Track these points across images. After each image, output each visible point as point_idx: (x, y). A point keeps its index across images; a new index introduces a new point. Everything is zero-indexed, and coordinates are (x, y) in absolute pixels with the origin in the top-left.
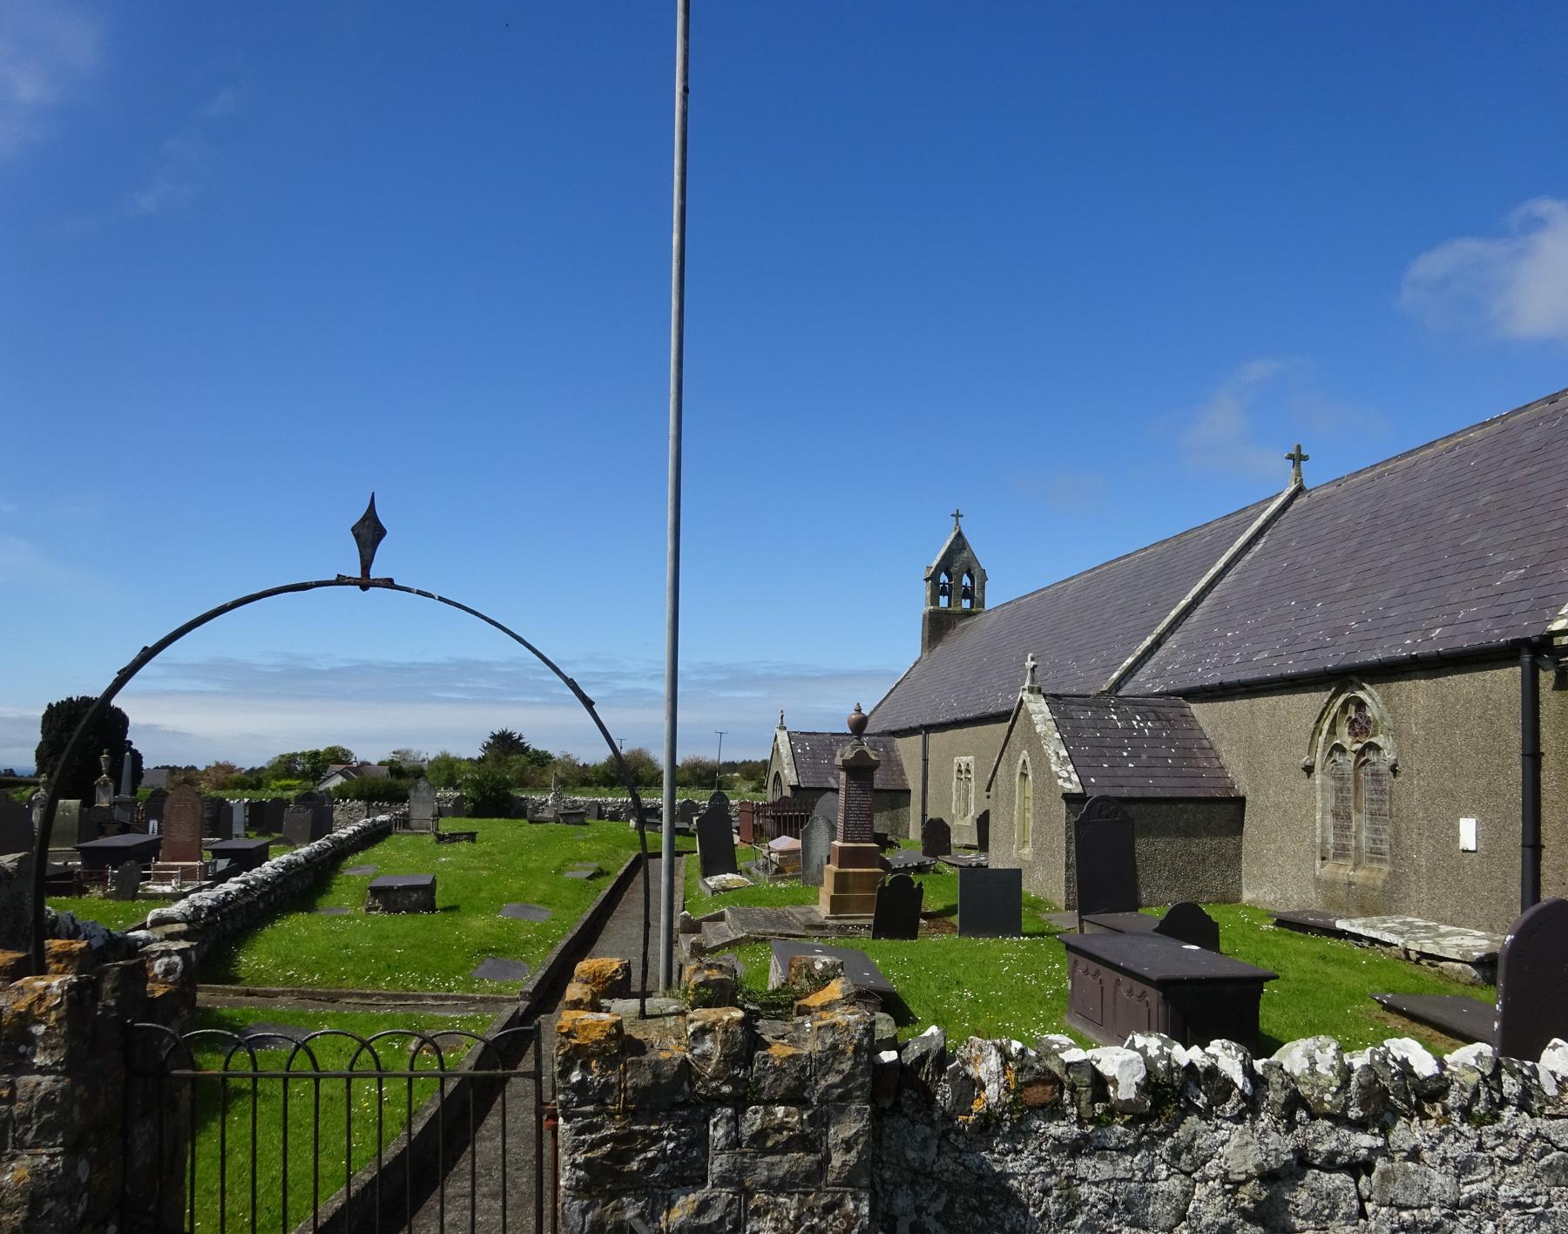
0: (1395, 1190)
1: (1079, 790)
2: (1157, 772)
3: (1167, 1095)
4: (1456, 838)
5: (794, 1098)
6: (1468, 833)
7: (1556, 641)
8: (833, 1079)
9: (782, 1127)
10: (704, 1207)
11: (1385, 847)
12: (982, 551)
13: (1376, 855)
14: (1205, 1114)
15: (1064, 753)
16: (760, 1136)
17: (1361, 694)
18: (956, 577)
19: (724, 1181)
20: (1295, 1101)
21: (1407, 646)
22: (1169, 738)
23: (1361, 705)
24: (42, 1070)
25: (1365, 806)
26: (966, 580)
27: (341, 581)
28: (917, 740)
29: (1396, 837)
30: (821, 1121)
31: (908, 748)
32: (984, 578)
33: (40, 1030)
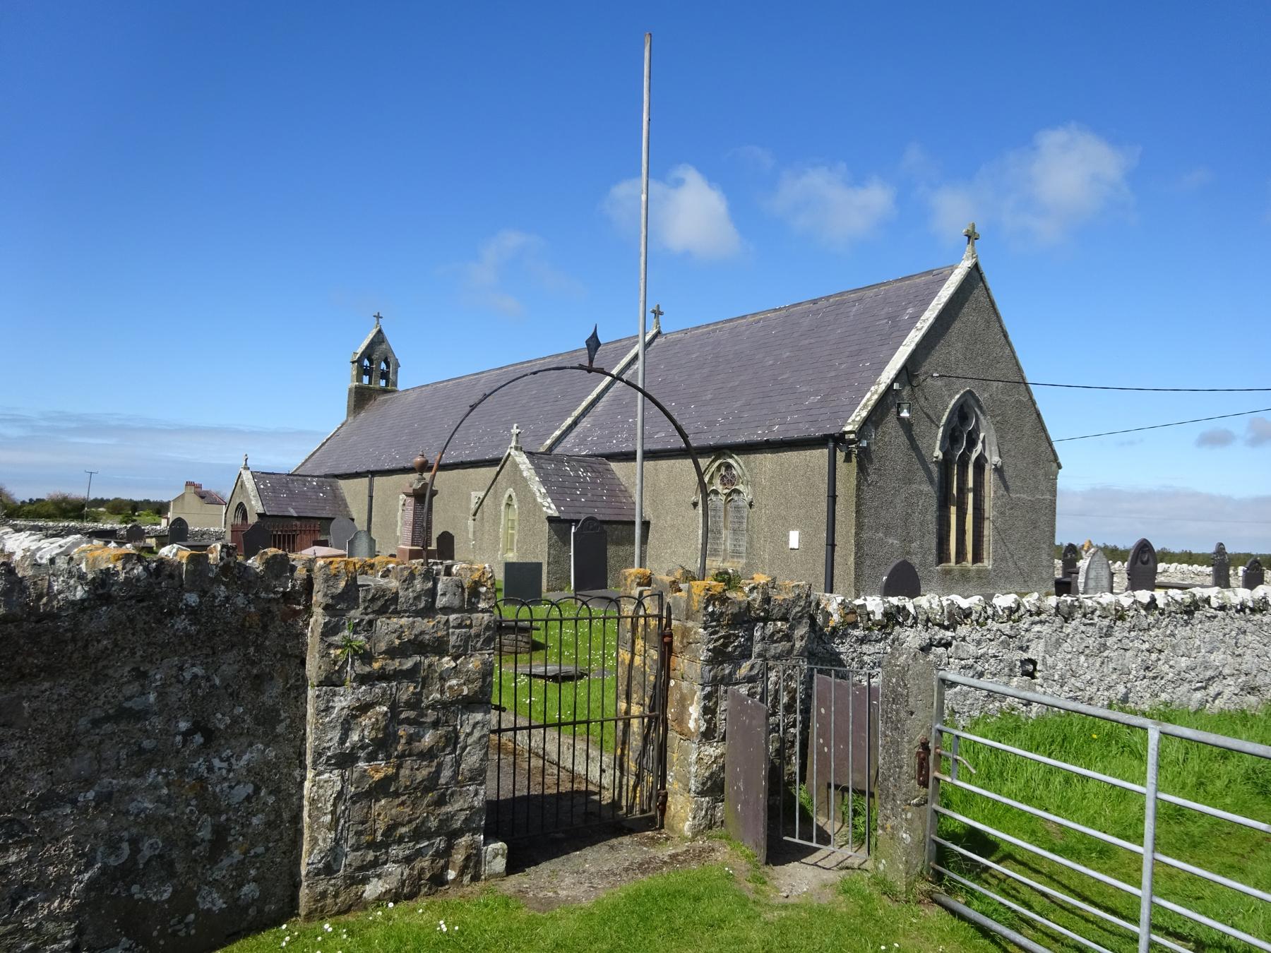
0: (960, 652)
1: (556, 514)
2: (598, 504)
3: (893, 617)
4: (787, 543)
5: (784, 619)
6: (794, 539)
7: (847, 436)
8: (798, 609)
9: (781, 630)
10: (752, 667)
11: (743, 549)
12: (397, 345)
13: (736, 554)
14: (901, 625)
15: (543, 490)
16: (773, 635)
17: (730, 461)
18: (375, 366)
19: (759, 655)
20: (928, 620)
21: (759, 435)
22: (602, 483)
23: (729, 467)
24: (483, 611)
25: (729, 525)
26: (383, 366)
27: (581, 367)
28: (366, 481)
29: (750, 542)
30: (792, 628)
31: (353, 491)
32: (397, 365)
33: (483, 589)
